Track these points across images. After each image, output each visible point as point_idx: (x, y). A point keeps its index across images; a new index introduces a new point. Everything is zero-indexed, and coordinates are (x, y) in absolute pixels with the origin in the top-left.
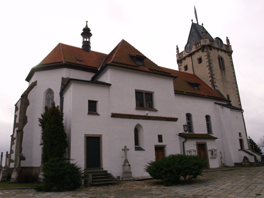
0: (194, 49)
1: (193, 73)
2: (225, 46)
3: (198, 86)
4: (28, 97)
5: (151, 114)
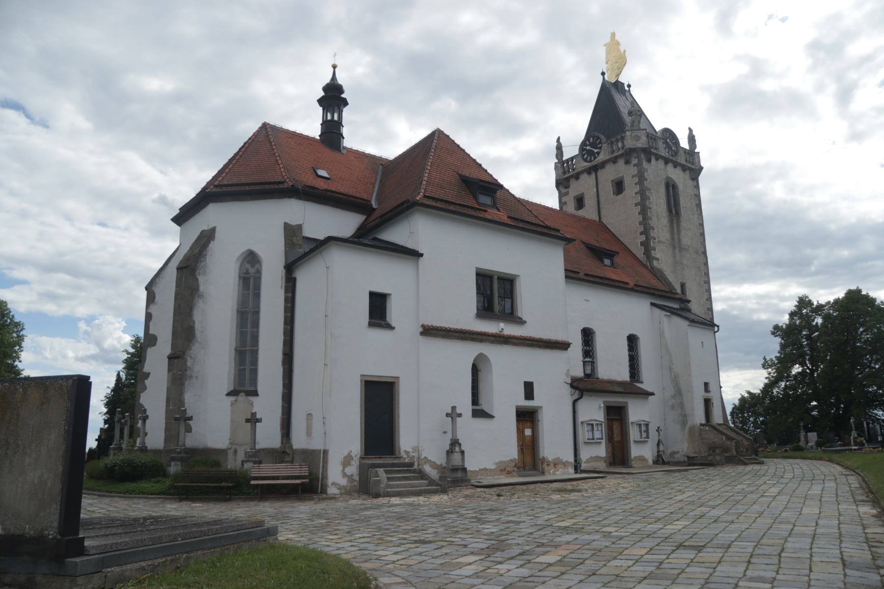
0: (602, 157)
1: (597, 219)
3: (613, 256)
5: (510, 330)
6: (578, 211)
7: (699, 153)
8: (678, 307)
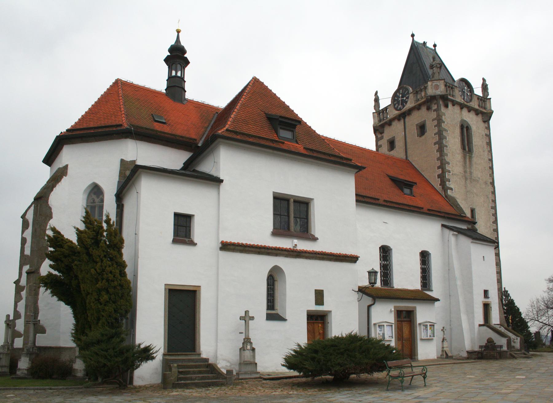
0: (410, 104)
2: (478, 99)
4: (49, 200)
5: (303, 245)
6: (390, 152)
8: (466, 228)
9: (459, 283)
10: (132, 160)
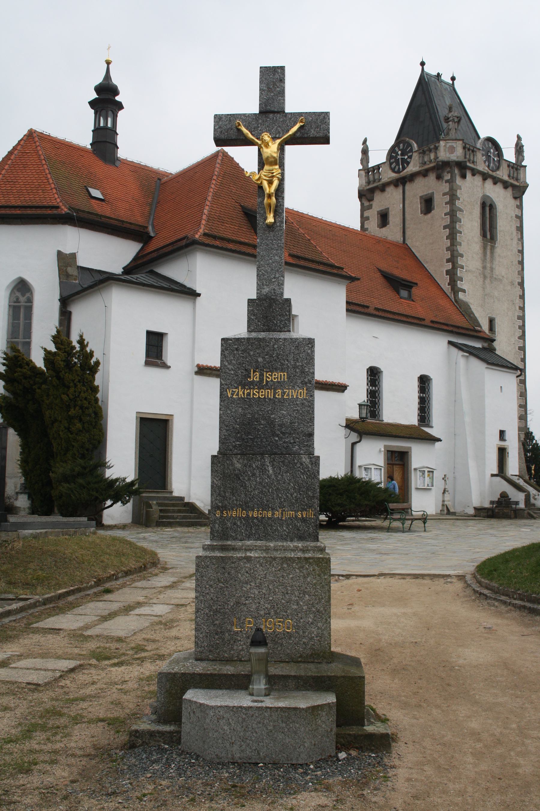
0: (413, 167)
1: (400, 239)
2: (509, 166)
3: (411, 287)
7: (525, 166)
8: (481, 347)
9: (467, 419)
10: (71, 252)
